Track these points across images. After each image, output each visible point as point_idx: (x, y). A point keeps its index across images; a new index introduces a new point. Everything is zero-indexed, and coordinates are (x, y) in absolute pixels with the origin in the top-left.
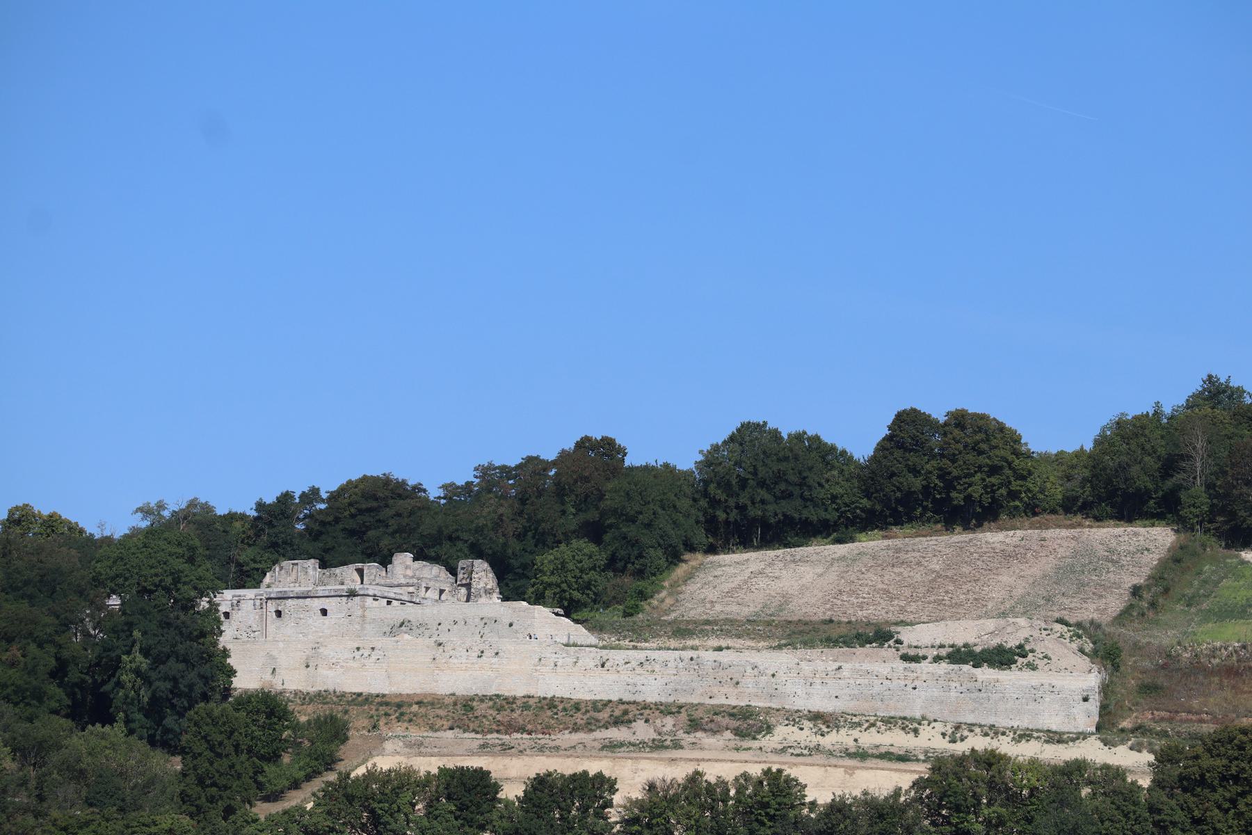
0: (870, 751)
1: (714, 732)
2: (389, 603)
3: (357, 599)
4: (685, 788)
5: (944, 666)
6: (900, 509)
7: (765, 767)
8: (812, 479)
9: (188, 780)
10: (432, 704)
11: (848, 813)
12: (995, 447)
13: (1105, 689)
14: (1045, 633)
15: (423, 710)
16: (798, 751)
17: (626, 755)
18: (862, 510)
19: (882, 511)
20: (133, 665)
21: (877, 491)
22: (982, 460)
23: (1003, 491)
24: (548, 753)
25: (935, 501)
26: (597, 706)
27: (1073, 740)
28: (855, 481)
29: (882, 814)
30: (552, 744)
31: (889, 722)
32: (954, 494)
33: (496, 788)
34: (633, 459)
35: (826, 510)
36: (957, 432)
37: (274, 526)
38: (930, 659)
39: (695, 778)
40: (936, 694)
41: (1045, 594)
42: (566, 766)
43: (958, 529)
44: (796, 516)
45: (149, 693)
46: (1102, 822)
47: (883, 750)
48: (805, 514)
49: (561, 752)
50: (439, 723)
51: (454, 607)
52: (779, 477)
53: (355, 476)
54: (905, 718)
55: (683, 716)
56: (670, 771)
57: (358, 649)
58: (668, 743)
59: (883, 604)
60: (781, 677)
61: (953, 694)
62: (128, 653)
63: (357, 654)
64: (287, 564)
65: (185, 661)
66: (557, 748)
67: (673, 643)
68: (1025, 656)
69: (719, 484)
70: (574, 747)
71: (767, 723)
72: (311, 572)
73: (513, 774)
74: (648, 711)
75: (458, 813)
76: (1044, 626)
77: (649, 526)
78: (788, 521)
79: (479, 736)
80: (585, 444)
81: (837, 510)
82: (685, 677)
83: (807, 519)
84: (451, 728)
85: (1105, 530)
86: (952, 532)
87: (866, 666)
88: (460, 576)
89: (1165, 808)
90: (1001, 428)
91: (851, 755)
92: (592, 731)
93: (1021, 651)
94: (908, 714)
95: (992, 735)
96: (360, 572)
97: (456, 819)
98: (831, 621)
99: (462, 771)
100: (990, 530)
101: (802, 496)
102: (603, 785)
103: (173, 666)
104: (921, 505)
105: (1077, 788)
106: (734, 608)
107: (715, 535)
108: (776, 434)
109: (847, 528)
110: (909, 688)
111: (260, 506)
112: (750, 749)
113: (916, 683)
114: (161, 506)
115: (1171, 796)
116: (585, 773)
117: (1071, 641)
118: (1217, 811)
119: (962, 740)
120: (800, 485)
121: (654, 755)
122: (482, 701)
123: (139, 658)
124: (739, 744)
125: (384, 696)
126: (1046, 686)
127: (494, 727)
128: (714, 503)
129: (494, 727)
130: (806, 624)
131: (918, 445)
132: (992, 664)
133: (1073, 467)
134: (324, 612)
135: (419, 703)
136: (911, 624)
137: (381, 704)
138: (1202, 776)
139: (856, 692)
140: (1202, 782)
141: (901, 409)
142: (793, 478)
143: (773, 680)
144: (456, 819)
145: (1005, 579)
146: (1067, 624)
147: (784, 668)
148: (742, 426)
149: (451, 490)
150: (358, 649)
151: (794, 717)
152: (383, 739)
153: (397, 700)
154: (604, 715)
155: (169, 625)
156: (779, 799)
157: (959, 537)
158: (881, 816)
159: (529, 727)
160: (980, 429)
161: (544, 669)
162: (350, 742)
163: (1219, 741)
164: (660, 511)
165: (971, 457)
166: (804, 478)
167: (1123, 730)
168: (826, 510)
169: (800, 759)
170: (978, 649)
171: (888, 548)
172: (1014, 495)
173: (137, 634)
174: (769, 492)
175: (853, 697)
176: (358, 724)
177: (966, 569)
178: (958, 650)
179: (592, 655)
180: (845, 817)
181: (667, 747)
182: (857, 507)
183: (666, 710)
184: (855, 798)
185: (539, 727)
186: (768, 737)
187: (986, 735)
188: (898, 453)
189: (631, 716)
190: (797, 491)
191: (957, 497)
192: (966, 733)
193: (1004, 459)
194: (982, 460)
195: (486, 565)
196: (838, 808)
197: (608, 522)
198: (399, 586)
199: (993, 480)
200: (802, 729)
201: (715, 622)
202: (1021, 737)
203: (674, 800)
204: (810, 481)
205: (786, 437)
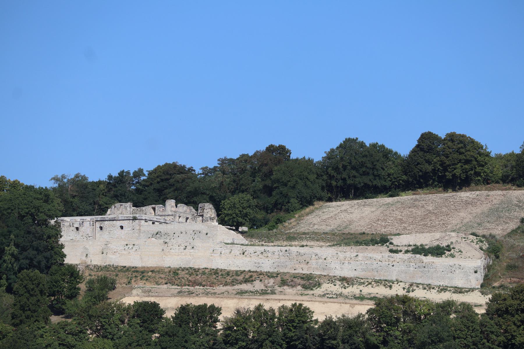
0: (366, 296)
1: (293, 286)
2: (153, 223)
3: (137, 221)
4: (254, 312)
5: (409, 255)
6: (422, 181)
7: (294, 302)
8: (378, 165)
9: (16, 307)
10: (159, 272)
11: (333, 326)
12: (469, 151)
13: (488, 268)
14: (464, 239)
15: (154, 275)
16: (331, 296)
17: (248, 297)
18: (403, 181)
19: (413, 181)
20: (10, 252)
21: (410, 172)
22: (462, 157)
23: (472, 172)
24: (210, 295)
25: (439, 177)
26: (238, 273)
27: (467, 292)
28: (400, 167)
29: (352, 325)
30: (213, 291)
31: (378, 282)
32: (447, 174)
33: (163, 312)
34: (293, 156)
35: (385, 181)
36: (450, 143)
37: (117, 187)
38: (403, 252)
39: (259, 308)
40: (403, 269)
41: (479, 221)
42: (196, 301)
43: (450, 190)
44: (370, 184)
45: (18, 266)
46: (456, 331)
47: (372, 296)
48: (375, 183)
49: (216, 295)
50: (161, 281)
51: (198, 225)
52: (363, 164)
53: (162, 164)
54: (386, 280)
55: (279, 278)
56: (249, 304)
57: (127, 245)
58: (269, 291)
59: (397, 224)
60: (329, 260)
61: (412, 269)
62: (8, 246)
63: (126, 247)
64: (118, 205)
65: (37, 249)
66: (215, 293)
67: (285, 243)
68: (449, 251)
69: (333, 168)
70: (223, 293)
71: (319, 282)
72: (128, 209)
73: (170, 304)
74: (262, 276)
75: (142, 324)
76: (464, 236)
77: (293, 187)
78: (366, 186)
79: (179, 287)
80: (271, 149)
81: (390, 181)
82: (283, 259)
83: (375, 185)
84: (166, 284)
85: (520, 191)
86: (447, 192)
87: (370, 255)
88: (199, 211)
89: (488, 324)
90: (472, 141)
91: (356, 298)
92: (234, 285)
93: (448, 248)
94: (389, 278)
95: (428, 289)
96: (154, 209)
97: (141, 326)
98: (364, 233)
99: (146, 304)
100: (465, 191)
101: (373, 174)
102: (215, 310)
103: (31, 253)
104: (431, 179)
105: (449, 314)
106: (324, 227)
107: (331, 192)
108: (362, 145)
109: (395, 189)
110: (390, 266)
111: (110, 177)
112: (308, 294)
113: (394, 263)
114: (63, 177)
115: (491, 319)
116: (205, 305)
117: (477, 244)
118: (513, 326)
119: (413, 291)
120: (373, 169)
121: (261, 297)
122: (183, 270)
123: (14, 248)
124: (303, 292)
125: (136, 267)
126: (457, 265)
127: (187, 283)
128: (331, 177)
129: (187, 283)
130: (352, 234)
131: (430, 150)
132: (433, 254)
133: (508, 161)
134: (122, 227)
135: (152, 271)
136: (399, 234)
137: (134, 272)
138: (507, 309)
139: (365, 267)
140: (507, 312)
141: (423, 132)
142: (369, 165)
143: (325, 261)
144: (141, 326)
145: (462, 214)
146: (476, 236)
147: (330, 255)
148: (346, 139)
149: (206, 171)
150: (127, 245)
151: (332, 280)
152: (132, 289)
153: (142, 270)
154: (240, 278)
155: (29, 232)
156: (299, 318)
157: (450, 194)
158: (350, 327)
159: (204, 283)
160: (461, 142)
161: (215, 255)
162: (117, 290)
163: (517, 291)
164: (299, 181)
165: (456, 156)
166: (375, 165)
167: (494, 287)
168: (385, 181)
169: (332, 300)
170: (427, 247)
171: (412, 199)
172: (477, 174)
173: (12, 236)
174: (359, 172)
175: (363, 270)
176: (121, 282)
177: (444, 209)
178: (418, 248)
179: (239, 248)
180: (331, 327)
181: (268, 294)
182: (400, 180)
183: (270, 275)
184: (339, 318)
185: (209, 283)
186: (318, 289)
187: (425, 289)
188: (421, 153)
189: (253, 278)
190: (371, 172)
191: (449, 175)
192: (415, 288)
193: (472, 156)
194: (462, 157)
195: (211, 206)
196: (329, 323)
197: (275, 185)
198: (168, 215)
199: (466, 166)
200: (335, 285)
201: (308, 234)
202: (442, 290)
203: (249, 318)
204: (377, 167)
205: (368, 145)
